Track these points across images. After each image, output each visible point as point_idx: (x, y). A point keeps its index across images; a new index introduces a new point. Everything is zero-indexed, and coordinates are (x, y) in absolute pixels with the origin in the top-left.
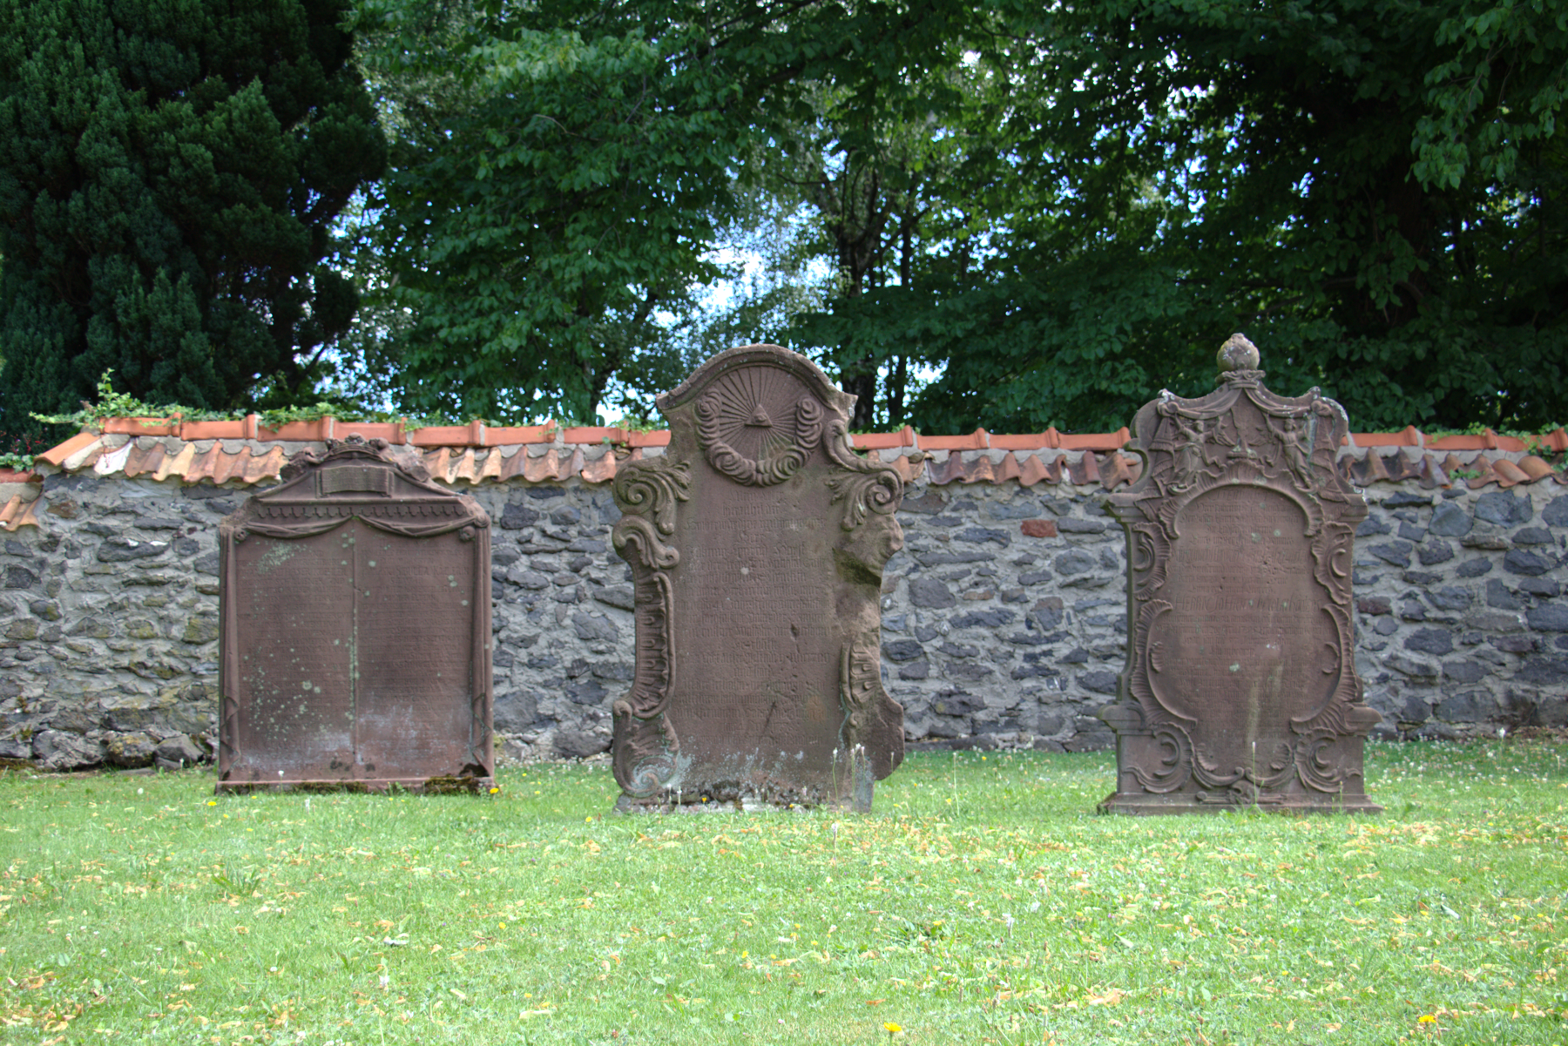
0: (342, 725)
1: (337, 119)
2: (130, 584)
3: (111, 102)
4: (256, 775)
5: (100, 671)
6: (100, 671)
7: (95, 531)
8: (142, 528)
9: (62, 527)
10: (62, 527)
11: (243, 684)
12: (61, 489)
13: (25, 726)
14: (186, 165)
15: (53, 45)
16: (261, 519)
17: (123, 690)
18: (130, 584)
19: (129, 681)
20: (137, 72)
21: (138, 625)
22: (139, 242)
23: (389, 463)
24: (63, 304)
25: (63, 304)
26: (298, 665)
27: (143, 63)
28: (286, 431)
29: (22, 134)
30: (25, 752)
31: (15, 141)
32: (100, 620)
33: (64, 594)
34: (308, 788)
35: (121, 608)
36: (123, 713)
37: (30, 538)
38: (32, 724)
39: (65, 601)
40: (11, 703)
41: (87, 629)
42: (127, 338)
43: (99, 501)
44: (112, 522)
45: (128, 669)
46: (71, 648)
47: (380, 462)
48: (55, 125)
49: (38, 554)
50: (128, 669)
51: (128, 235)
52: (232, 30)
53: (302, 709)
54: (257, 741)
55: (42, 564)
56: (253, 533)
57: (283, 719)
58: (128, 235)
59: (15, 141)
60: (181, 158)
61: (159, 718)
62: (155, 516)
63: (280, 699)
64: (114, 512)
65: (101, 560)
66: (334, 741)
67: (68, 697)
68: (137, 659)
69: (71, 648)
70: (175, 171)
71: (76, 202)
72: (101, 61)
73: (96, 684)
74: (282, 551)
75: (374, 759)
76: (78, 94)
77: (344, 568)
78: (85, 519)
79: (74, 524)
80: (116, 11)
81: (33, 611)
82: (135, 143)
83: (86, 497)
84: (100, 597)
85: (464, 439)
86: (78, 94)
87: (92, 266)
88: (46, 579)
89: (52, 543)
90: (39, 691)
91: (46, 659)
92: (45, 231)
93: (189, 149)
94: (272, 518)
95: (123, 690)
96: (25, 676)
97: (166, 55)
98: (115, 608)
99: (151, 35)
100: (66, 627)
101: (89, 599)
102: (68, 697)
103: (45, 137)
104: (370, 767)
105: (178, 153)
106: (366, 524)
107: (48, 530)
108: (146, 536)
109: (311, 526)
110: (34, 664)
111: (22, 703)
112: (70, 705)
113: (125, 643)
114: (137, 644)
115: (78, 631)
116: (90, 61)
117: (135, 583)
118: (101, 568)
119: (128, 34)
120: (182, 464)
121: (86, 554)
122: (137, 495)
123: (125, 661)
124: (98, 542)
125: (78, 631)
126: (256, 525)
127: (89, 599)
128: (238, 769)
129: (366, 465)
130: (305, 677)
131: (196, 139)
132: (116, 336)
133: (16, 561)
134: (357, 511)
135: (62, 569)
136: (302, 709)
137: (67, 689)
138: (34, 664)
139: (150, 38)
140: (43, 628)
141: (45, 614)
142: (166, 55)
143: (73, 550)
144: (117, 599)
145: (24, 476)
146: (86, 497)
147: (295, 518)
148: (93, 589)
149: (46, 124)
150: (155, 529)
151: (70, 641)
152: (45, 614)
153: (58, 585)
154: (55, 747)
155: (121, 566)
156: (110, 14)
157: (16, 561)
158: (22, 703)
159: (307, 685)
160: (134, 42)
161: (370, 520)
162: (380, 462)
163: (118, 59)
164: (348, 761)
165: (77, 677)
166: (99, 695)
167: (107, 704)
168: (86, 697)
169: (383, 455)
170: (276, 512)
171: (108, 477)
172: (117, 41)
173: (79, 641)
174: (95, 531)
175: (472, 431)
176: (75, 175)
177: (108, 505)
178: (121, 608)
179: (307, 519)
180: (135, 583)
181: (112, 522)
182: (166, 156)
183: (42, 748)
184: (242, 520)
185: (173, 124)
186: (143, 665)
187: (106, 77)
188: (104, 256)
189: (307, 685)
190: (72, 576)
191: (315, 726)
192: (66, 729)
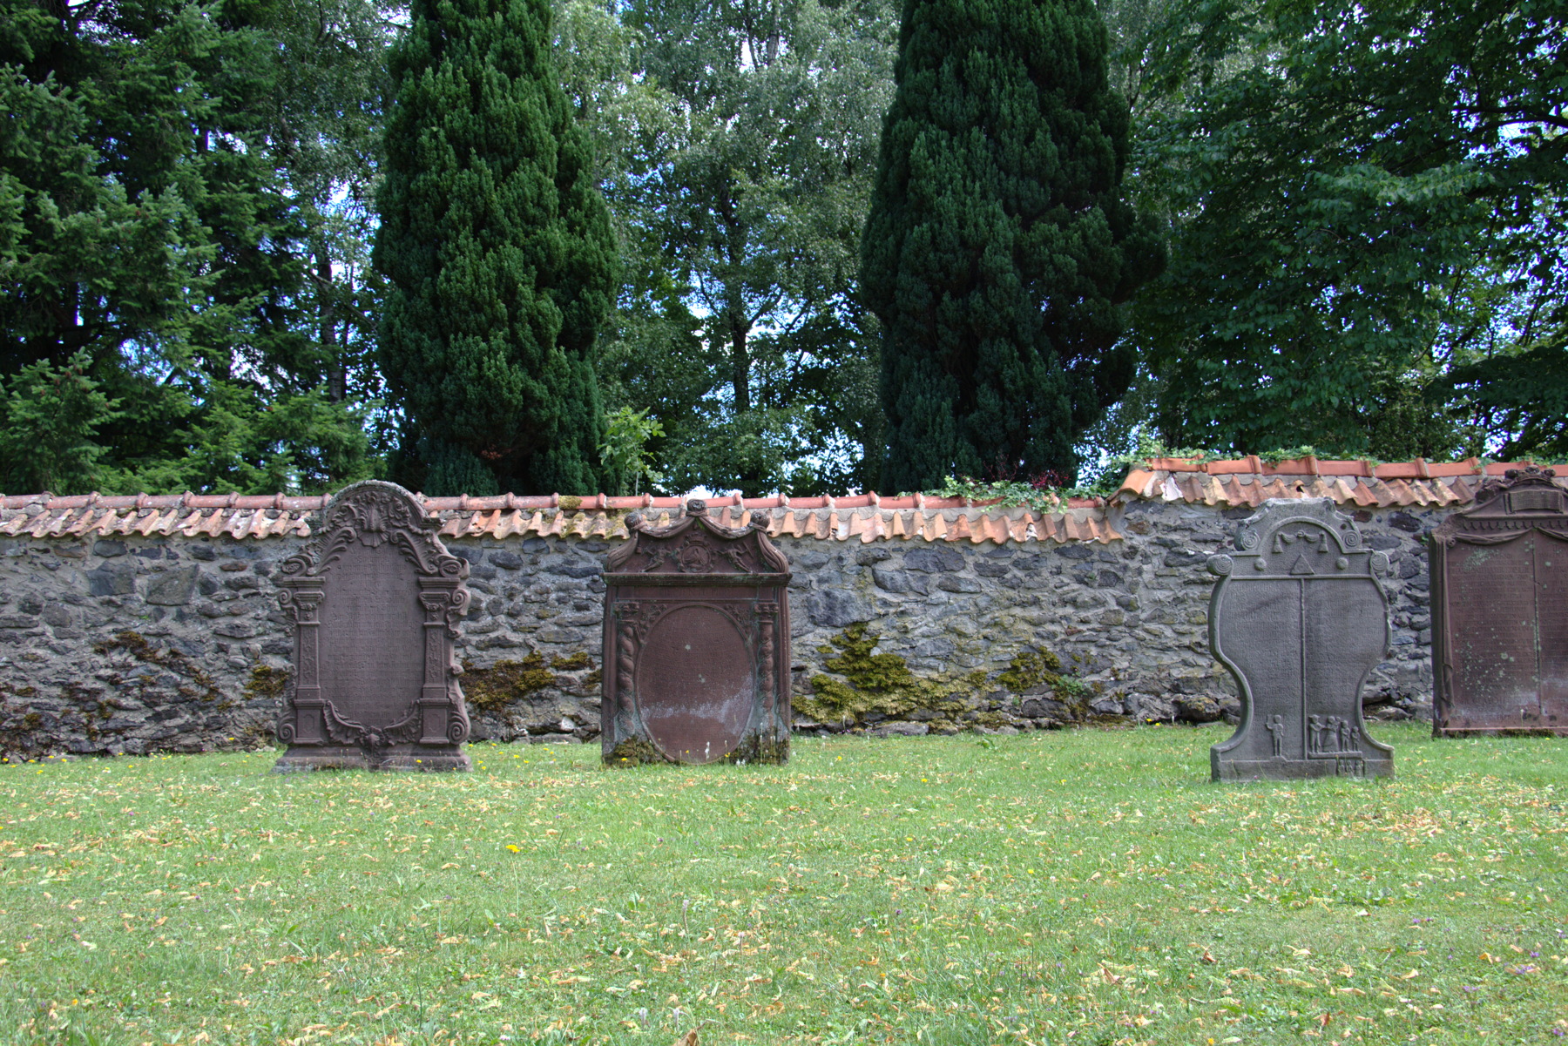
0: (1531, 686)
1: (1142, 234)
2: (1189, 583)
3: (1006, 229)
4: (1467, 724)
5: (1169, 649)
6: (1169, 649)
7: (1163, 543)
8: (1197, 541)
9: (1138, 541)
10: (1138, 541)
11: (1455, 655)
12: (1138, 512)
13: (1118, 690)
14: (1057, 270)
15: (958, 183)
16: (1466, 530)
17: (1185, 663)
18: (1189, 583)
19: (1189, 656)
20: (1013, 202)
21: (1195, 614)
22: (1020, 329)
23: (1558, 488)
24: (949, 376)
25: (949, 376)
26: (1497, 641)
27: (1017, 196)
28: (1281, 467)
29: (937, 250)
30: (1119, 709)
31: (931, 256)
32: (1167, 610)
33: (1141, 591)
34: (1510, 734)
35: (1183, 601)
36: (1188, 680)
37: (1117, 549)
38: (1122, 688)
39: (1142, 596)
40: (1107, 673)
41: (1157, 617)
42: (1012, 400)
43: (1165, 521)
44: (1175, 537)
45: (1189, 648)
46: (1147, 631)
47: (1552, 486)
48: (964, 243)
49: (1122, 561)
50: (1189, 648)
51: (1013, 325)
52: (1074, 170)
53: (1501, 673)
54: (1468, 698)
55: (1125, 568)
56: (1459, 541)
57: (1487, 681)
58: (1013, 325)
59: (931, 256)
60: (1054, 265)
61: (1212, 685)
62: (1206, 532)
63: (1485, 667)
64: (1175, 530)
65: (1167, 565)
66: (1524, 698)
67: (1146, 668)
68: (1195, 640)
69: (1147, 631)
70: (1050, 275)
71: (976, 300)
72: (991, 195)
73: (1166, 659)
74: (1481, 554)
75: (1555, 711)
76: (981, 220)
77: (1527, 568)
78: (1154, 535)
79: (1147, 539)
80: (1001, 159)
81: (1118, 604)
82: (1020, 255)
83: (1155, 518)
84: (1167, 593)
85: (1413, 473)
86: (981, 220)
87: (984, 346)
88: (1128, 579)
89: (1132, 552)
90: (1126, 664)
91: (1130, 640)
92: (946, 323)
93: (1059, 258)
94: (1474, 529)
95: (1185, 663)
96: (1115, 652)
97: (1034, 192)
98: (1178, 601)
99: (1023, 175)
100: (1143, 616)
101: (1160, 595)
102: (1146, 668)
103: (954, 252)
104: (1552, 718)
105: (1051, 261)
106: (1542, 533)
107: (1129, 543)
108: (1200, 547)
109: (1504, 535)
110: (1121, 644)
111: (1115, 673)
112: (1149, 674)
113: (1186, 628)
114: (1194, 629)
115: (1151, 619)
116: (984, 196)
117: (1193, 582)
118: (1167, 571)
119: (1008, 175)
120: (1216, 492)
121: (1155, 560)
122: (1191, 516)
123: (1186, 641)
124: (1164, 552)
125: (1151, 619)
126: (1461, 535)
127: (1160, 595)
128: (1453, 719)
129: (1543, 489)
130: (1503, 649)
131: (1065, 251)
132: (1002, 399)
133: (1106, 566)
134: (1537, 525)
135: (1140, 572)
136: (1501, 673)
137: (1146, 662)
138: (1121, 644)
139: (1022, 178)
140: (1126, 617)
141: (1128, 606)
142: (1034, 192)
143: (1146, 558)
144: (1180, 595)
145: (1090, 503)
146: (1155, 518)
147: (1491, 530)
148: (1162, 588)
149: (956, 243)
150: (1205, 542)
151: (1147, 626)
152: (1128, 606)
153: (1137, 584)
154: (1141, 706)
155: (1183, 570)
156: (995, 160)
157: (1106, 566)
158: (1115, 673)
159: (1504, 656)
160: (1013, 180)
161: (1547, 530)
162: (1552, 486)
163: (1003, 194)
164: (1535, 713)
165: (1153, 653)
166: (1169, 667)
167: (1175, 673)
168: (1159, 669)
169: (1554, 481)
170: (1477, 525)
171: (1170, 503)
172: (1000, 180)
173: (1152, 626)
174: (1163, 543)
175: (1419, 467)
176: (977, 279)
177: (1171, 523)
178: (1183, 601)
179: (1500, 530)
180: (1193, 582)
181: (1175, 537)
182: (1041, 264)
183: (1133, 706)
184: (1450, 532)
185: (1047, 241)
186: (1199, 644)
187: (997, 207)
188: (992, 340)
189: (1504, 656)
190: (1147, 577)
191: (1511, 686)
192: (1147, 692)
